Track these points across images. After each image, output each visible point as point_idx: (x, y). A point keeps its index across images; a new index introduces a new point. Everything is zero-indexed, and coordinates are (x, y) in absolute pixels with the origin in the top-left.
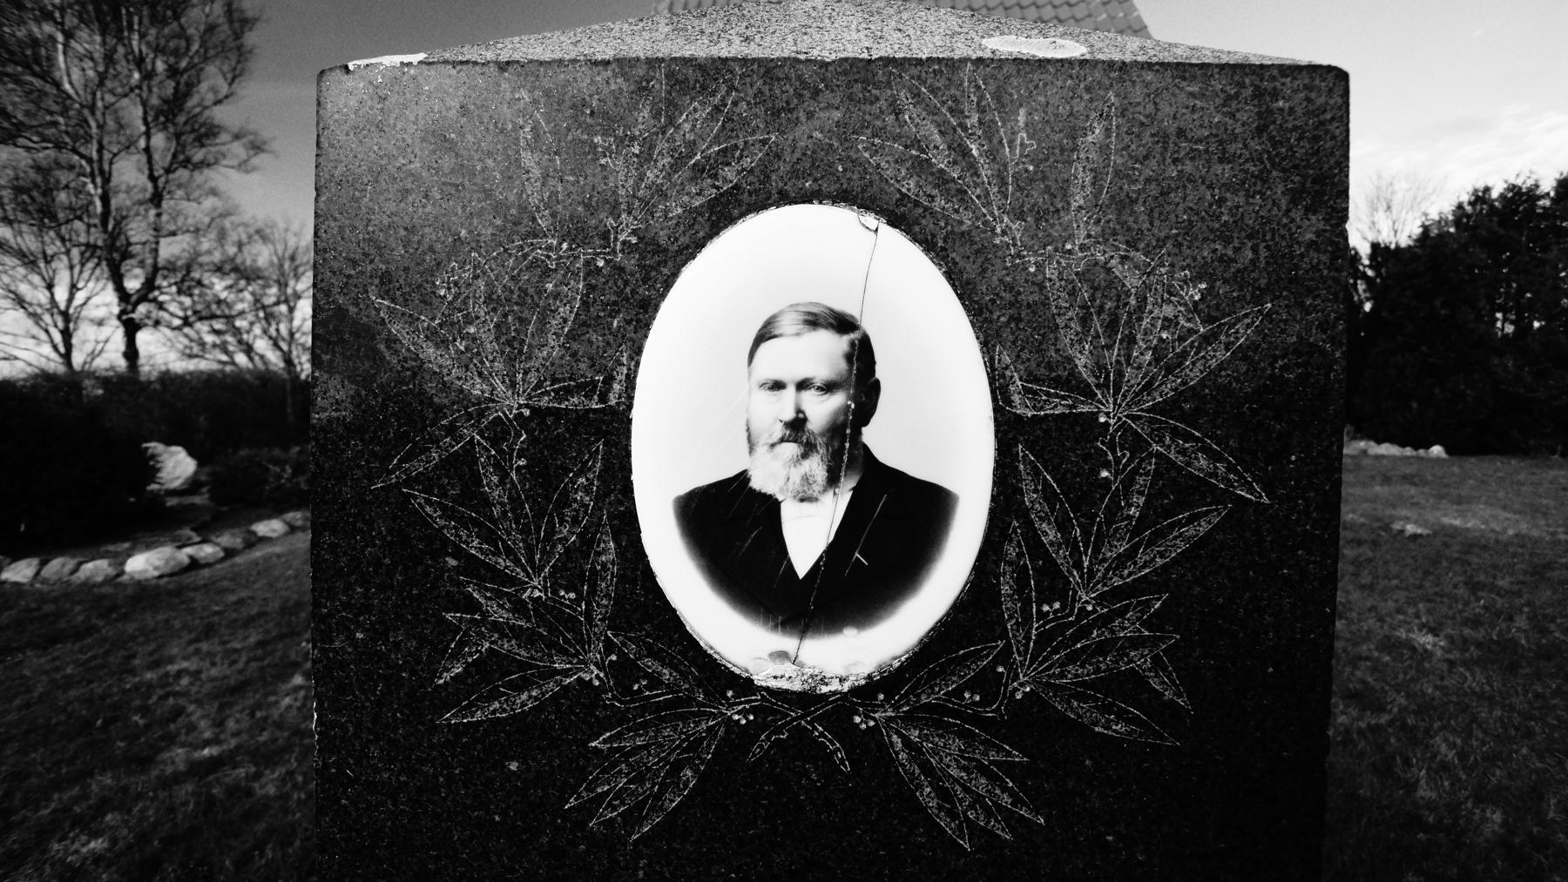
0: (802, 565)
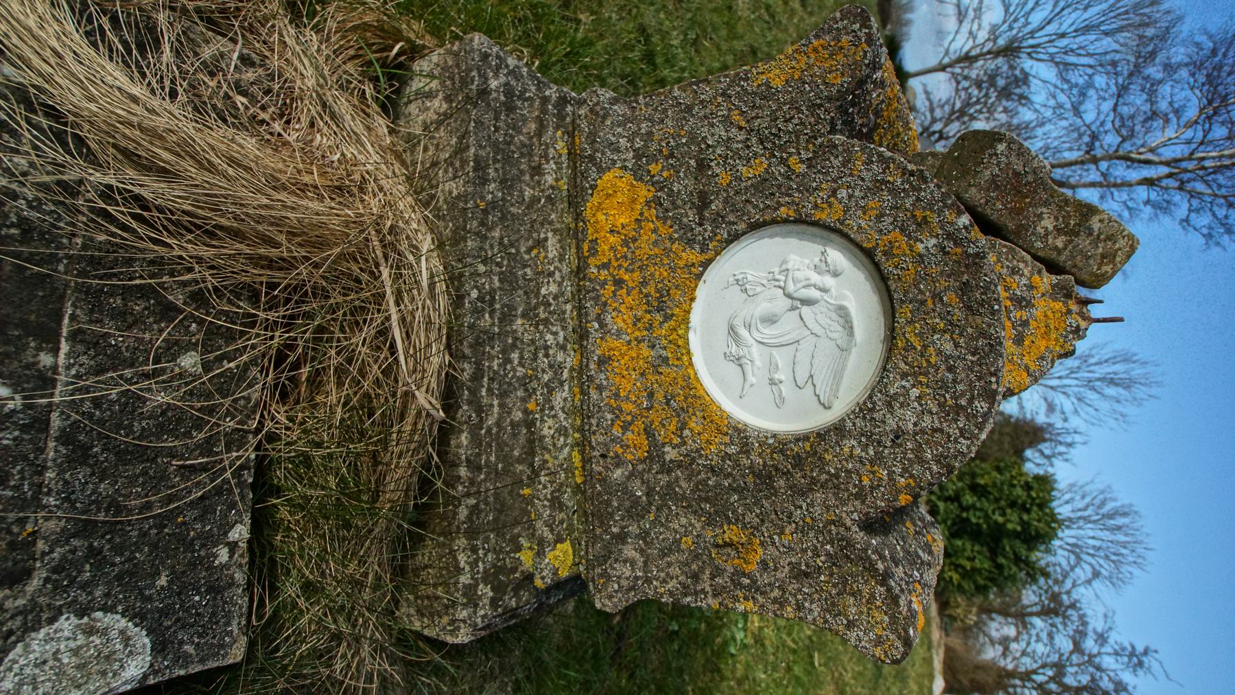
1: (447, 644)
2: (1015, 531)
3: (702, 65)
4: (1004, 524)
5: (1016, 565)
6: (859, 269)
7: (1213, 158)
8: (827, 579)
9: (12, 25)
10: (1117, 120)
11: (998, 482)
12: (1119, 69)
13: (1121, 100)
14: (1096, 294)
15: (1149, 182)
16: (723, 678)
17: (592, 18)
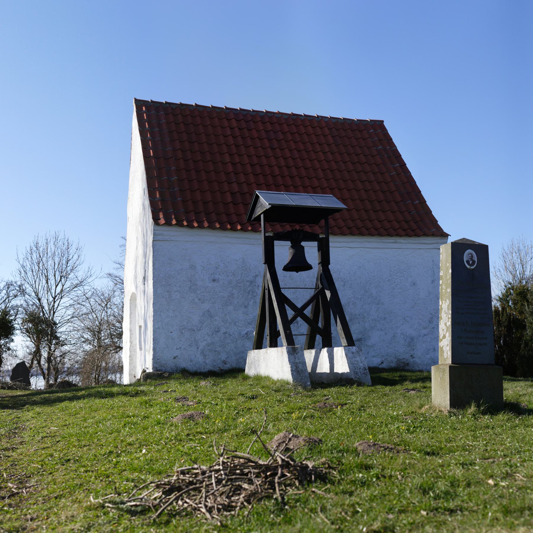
1: (371, 377)
2: (284, 499)
3: (24, 434)
4: (232, 482)
5: (101, 338)
6: (461, 240)
7: (7, 400)
8: (254, 450)
9: (147, 309)
10: (237, 493)
11: (255, 476)
12: (145, 527)
13: (306, 504)
14: (80, 273)
15: (128, 416)
16: (329, 494)
17: (365, 489)
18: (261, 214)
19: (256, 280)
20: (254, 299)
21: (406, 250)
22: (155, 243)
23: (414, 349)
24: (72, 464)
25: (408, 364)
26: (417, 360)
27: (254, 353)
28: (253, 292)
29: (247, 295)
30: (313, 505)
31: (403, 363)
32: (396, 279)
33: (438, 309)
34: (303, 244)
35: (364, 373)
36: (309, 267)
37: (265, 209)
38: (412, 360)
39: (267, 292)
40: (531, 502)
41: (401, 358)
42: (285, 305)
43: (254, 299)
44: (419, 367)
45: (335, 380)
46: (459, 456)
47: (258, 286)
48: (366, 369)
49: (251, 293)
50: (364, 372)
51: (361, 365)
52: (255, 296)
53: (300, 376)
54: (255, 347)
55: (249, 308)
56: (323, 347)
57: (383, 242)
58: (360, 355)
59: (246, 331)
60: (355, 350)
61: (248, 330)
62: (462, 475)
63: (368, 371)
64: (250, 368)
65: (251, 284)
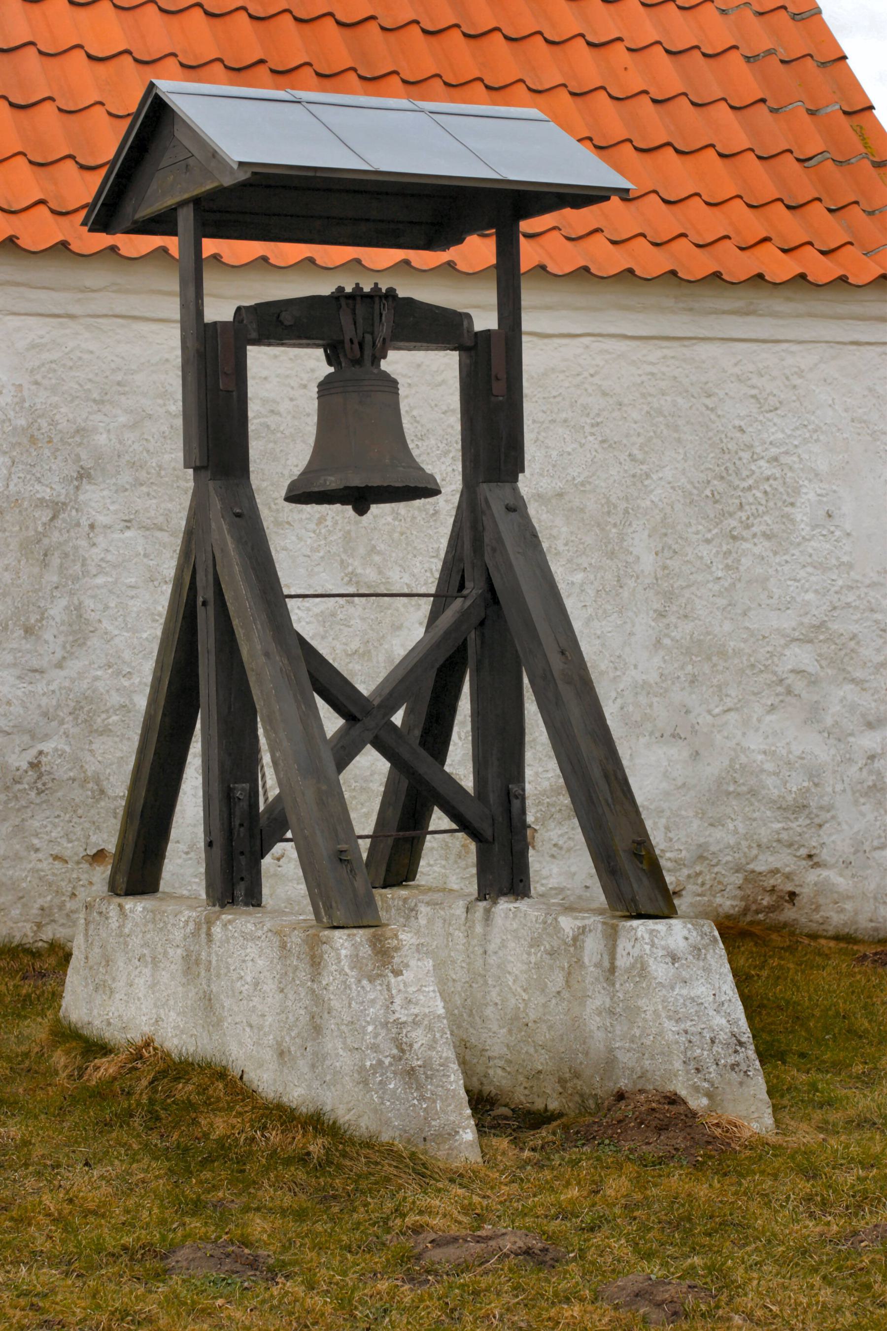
0: (436, 808)
18: (183, 204)
19: (81, 497)
20: (72, 593)
21: (794, 348)
22: (60, 246)
23: (820, 826)
24: (190, 1093)
25: (792, 895)
26: (602, 947)
27: (420, 455)
28: (66, 555)
29: (36, 570)
30: (812, 496)
31: (773, 890)
32: (750, 488)
33: (518, 895)
34: (332, 370)
35: (733, 1067)
36: (429, 490)
37: (209, 186)
38: (812, 876)
39: (206, 620)
40: (882, 708)
41: (759, 869)
42: (404, 707)
43: (72, 593)
44: (842, 911)
45: (180, 1054)
46: (826, 999)
47: (92, 526)
48: (741, 1044)
49: (55, 561)
50: (731, 1060)
51: (720, 1021)
52: (75, 579)
53: (422, 1098)
54: (122, 881)
55: (48, 636)
56: (278, 798)
57: (691, 310)
58: (707, 970)
59: (33, 752)
60: (682, 944)
61: (121, 536)
62: (709, 1200)
63: (751, 1053)
64: (288, 586)
65: (54, 518)
